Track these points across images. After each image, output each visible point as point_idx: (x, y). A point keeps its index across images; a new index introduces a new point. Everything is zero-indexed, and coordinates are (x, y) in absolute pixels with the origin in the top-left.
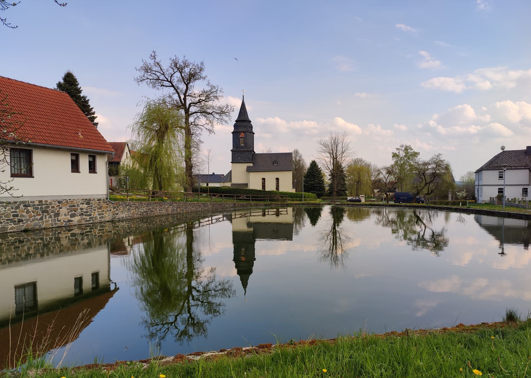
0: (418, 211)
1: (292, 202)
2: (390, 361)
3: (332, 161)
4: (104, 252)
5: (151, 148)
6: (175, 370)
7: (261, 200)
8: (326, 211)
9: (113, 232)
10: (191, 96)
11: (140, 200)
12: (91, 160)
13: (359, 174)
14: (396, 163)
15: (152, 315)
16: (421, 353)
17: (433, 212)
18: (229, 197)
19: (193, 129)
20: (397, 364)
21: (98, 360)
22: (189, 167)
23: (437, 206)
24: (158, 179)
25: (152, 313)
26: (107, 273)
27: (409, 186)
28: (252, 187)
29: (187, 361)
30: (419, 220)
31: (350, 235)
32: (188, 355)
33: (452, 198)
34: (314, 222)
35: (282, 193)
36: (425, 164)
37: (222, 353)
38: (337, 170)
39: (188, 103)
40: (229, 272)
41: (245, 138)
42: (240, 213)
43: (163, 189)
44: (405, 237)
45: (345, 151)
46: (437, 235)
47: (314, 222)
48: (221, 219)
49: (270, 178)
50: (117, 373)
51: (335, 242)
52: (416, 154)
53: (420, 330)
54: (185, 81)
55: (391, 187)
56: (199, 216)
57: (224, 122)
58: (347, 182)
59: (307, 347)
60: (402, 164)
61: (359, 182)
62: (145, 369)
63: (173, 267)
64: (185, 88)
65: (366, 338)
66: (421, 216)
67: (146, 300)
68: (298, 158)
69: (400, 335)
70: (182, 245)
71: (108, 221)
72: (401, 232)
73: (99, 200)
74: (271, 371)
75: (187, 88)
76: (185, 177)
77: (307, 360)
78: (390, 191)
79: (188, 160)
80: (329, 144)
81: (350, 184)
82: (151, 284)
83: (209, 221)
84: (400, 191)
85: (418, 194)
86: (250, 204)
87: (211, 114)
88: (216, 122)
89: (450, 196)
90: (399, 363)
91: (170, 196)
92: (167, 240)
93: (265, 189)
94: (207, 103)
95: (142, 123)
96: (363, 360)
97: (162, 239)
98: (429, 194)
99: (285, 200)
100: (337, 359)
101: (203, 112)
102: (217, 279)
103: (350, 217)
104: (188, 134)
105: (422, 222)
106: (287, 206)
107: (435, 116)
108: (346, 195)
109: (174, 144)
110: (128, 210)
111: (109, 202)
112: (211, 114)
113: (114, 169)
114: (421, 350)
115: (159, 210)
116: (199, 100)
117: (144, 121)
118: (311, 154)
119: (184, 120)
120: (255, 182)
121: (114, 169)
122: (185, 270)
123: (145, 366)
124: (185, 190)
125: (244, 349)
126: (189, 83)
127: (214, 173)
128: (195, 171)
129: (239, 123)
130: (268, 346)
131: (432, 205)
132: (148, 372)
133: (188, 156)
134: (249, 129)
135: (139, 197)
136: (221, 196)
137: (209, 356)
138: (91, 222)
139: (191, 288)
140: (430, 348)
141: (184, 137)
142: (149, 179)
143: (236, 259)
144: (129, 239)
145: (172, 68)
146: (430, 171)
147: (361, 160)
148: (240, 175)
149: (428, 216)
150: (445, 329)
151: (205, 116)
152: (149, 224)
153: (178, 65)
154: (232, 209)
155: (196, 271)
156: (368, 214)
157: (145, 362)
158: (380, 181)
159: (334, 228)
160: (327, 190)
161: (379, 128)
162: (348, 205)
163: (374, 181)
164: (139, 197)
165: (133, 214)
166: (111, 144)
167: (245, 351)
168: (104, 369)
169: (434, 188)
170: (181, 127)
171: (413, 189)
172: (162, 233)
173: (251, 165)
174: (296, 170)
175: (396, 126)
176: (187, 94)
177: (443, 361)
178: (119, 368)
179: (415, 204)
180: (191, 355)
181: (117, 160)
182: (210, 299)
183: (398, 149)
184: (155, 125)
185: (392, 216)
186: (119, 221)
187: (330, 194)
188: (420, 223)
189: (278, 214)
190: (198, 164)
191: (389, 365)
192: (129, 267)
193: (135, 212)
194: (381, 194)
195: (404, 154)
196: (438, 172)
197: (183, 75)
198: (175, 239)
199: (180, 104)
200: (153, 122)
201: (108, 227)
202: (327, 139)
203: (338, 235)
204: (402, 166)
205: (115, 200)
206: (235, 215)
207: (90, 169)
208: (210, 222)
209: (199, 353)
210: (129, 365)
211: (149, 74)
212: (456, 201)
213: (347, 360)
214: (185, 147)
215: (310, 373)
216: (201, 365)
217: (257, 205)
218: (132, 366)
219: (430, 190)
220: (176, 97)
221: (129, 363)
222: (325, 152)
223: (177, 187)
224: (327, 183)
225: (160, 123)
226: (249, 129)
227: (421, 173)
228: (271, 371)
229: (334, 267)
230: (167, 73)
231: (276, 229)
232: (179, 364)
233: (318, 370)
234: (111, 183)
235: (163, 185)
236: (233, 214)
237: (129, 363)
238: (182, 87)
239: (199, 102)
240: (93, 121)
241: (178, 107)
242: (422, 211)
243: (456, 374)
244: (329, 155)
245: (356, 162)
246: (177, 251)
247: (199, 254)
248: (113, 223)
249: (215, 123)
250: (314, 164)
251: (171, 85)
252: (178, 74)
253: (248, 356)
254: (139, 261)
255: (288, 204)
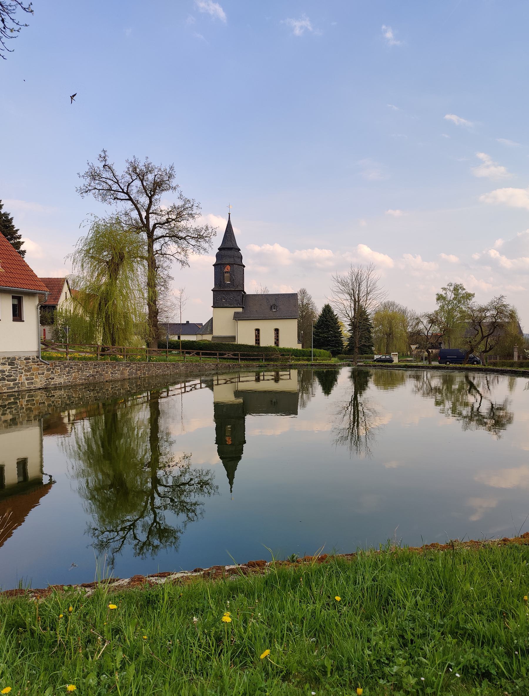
0: (471, 375)
1: (296, 363)
2: (428, 585)
3: (353, 305)
4: (35, 431)
5: (100, 287)
6: (131, 597)
7: (254, 360)
8: (344, 375)
9: (46, 403)
10: (156, 213)
11: (84, 358)
12: (16, 303)
13: (390, 323)
14: (442, 307)
15: (102, 519)
16: (472, 573)
17: (492, 376)
18: (211, 354)
19: (159, 260)
20: (437, 590)
21: (23, 585)
22: (154, 313)
23: (498, 368)
24: (110, 329)
25: (102, 517)
26: (38, 460)
27: (459, 341)
28: (240, 341)
29: (148, 586)
30: (472, 387)
31: (377, 408)
32: (149, 577)
33: (519, 357)
34: (327, 390)
35: (284, 350)
36: (482, 310)
37: (196, 574)
38: (360, 319)
39: (152, 223)
40: (210, 459)
41: (231, 273)
42: (224, 377)
43: (116, 344)
44: (454, 410)
45: (371, 291)
46: (497, 409)
47: (327, 390)
48: (198, 386)
49: (268, 328)
50: (50, 603)
51: (356, 420)
52: (469, 296)
53: (471, 541)
54: (148, 192)
55: (435, 342)
56: (167, 382)
57: (202, 251)
58: (373, 335)
59: (314, 565)
60: (449, 310)
61: (390, 335)
62: (88, 597)
63: (131, 453)
64: (147, 202)
65: (395, 553)
66: (475, 382)
67: (93, 498)
68: (305, 301)
69: (443, 548)
70: (143, 421)
71: (40, 389)
72: (448, 404)
73: (27, 359)
74: (263, 600)
75: (151, 202)
76: (148, 327)
77: (314, 584)
78: (433, 347)
79: (152, 304)
80: (349, 281)
81: (378, 337)
82: (100, 477)
83: (181, 388)
84: (447, 347)
85: (472, 351)
86: (239, 365)
87: (185, 238)
88: (192, 250)
89: (516, 354)
90: (440, 588)
91: (128, 354)
92: (123, 415)
93: (259, 343)
94: (179, 224)
95: (88, 251)
96: (392, 584)
97: (115, 415)
98: (488, 351)
99: (287, 359)
100: (355, 583)
101: (173, 236)
102: (192, 468)
103: (377, 383)
104: (152, 267)
105: (478, 392)
106: (290, 368)
107: (499, 242)
108: (373, 353)
109: (132, 280)
110: (68, 373)
111: (41, 361)
112: (185, 238)
113: (48, 315)
114: (472, 569)
115: (112, 373)
116: (167, 219)
117: (90, 249)
118: (324, 295)
119: (146, 247)
120: (245, 334)
121: (48, 315)
122: (148, 456)
123: (90, 591)
124: (148, 345)
125: (227, 568)
126: (154, 195)
127: (188, 322)
128: (162, 319)
129: (223, 252)
130: (261, 565)
131: (491, 367)
132: (93, 601)
133: (152, 297)
134: (238, 260)
135: (83, 355)
136: (198, 354)
137: (178, 578)
138: (16, 389)
139: (156, 482)
140: (484, 567)
141: (147, 271)
142: (97, 330)
143: (219, 441)
144: (69, 414)
145: (130, 174)
146: (488, 320)
147: (393, 304)
148: (225, 324)
149: (486, 381)
150: (504, 540)
151: (176, 242)
152: (98, 393)
153: (138, 170)
154: (213, 372)
155: (163, 459)
156: (402, 380)
157: (89, 586)
158: (419, 333)
159: (355, 398)
160: (346, 345)
161: (419, 259)
162: (374, 366)
163: (411, 333)
164: (83, 355)
165: (75, 378)
166: (44, 280)
167: (228, 571)
168: (32, 597)
169: (493, 343)
170: (142, 257)
171: (465, 344)
172: (115, 406)
173: (240, 310)
174: (302, 317)
175: (443, 255)
176: (151, 211)
177: (502, 586)
178: (52, 595)
179: (467, 366)
180: (152, 576)
181: (52, 303)
182: (183, 498)
183: (444, 289)
184: (105, 253)
185: (436, 382)
186: (55, 388)
187: (350, 351)
188: (474, 391)
189: (277, 379)
190: (166, 309)
191: (427, 591)
192: (71, 454)
193: (78, 376)
194: (421, 352)
195: (453, 296)
196: (499, 320)
197: (145, 184)
198: (133, 414)
199: (141, 225)
200: (103, 249)
201: (40, 397)
202: (346, 274)
203: (360, 408)
204: (450, 313)
205: (50, 358)
206: (218, 380)
207: (14, 315)
208: (183, 390)
209: (165, 573)
210: (67, 591)
211: (97, 182)
212: (524, 361)
213: (369, 583)
214: (148, 284)
215: (317, 602)
216: (167, 591)
217: (248, 366)
218: (70, 593)
219: (488, 346)
220: (135, 214)
221: (66, 588)
222: (343, 292)
223: (137, 341)
224: (346, 336)
225: (112, 251)
226: (238, 260)
227: (477, 323)
228: (263, 600)
229: (355, 453)
230: (123, 181)
231: (274, 400)
232: (137, 589)
233: (329, 597)
234: (45, 335)
235: (117, 339)
236: (215, 378)
237: (66, 588)
238: (144, 200)
239: (168, 221)
240: (18, 248)
241: (138, 229)
242: (476, 375)
243: (519, 604)
244: (348, 297)
245: (387, 306)
246: (136, 432)
247: (168, 434)
248: (47, 391)
249: (190, 250)
250: (327, 310)
251: (127, 198)
252: (138, 183)
253: (232, 578)
254: (83, 443)
255: (291, 365)
